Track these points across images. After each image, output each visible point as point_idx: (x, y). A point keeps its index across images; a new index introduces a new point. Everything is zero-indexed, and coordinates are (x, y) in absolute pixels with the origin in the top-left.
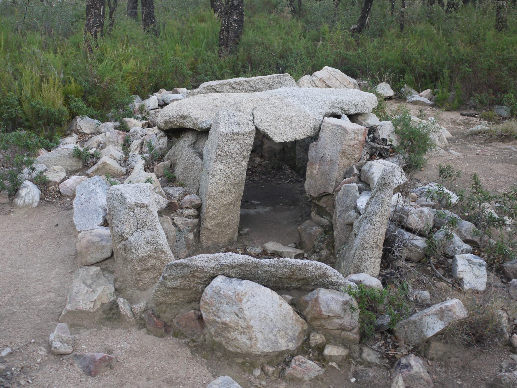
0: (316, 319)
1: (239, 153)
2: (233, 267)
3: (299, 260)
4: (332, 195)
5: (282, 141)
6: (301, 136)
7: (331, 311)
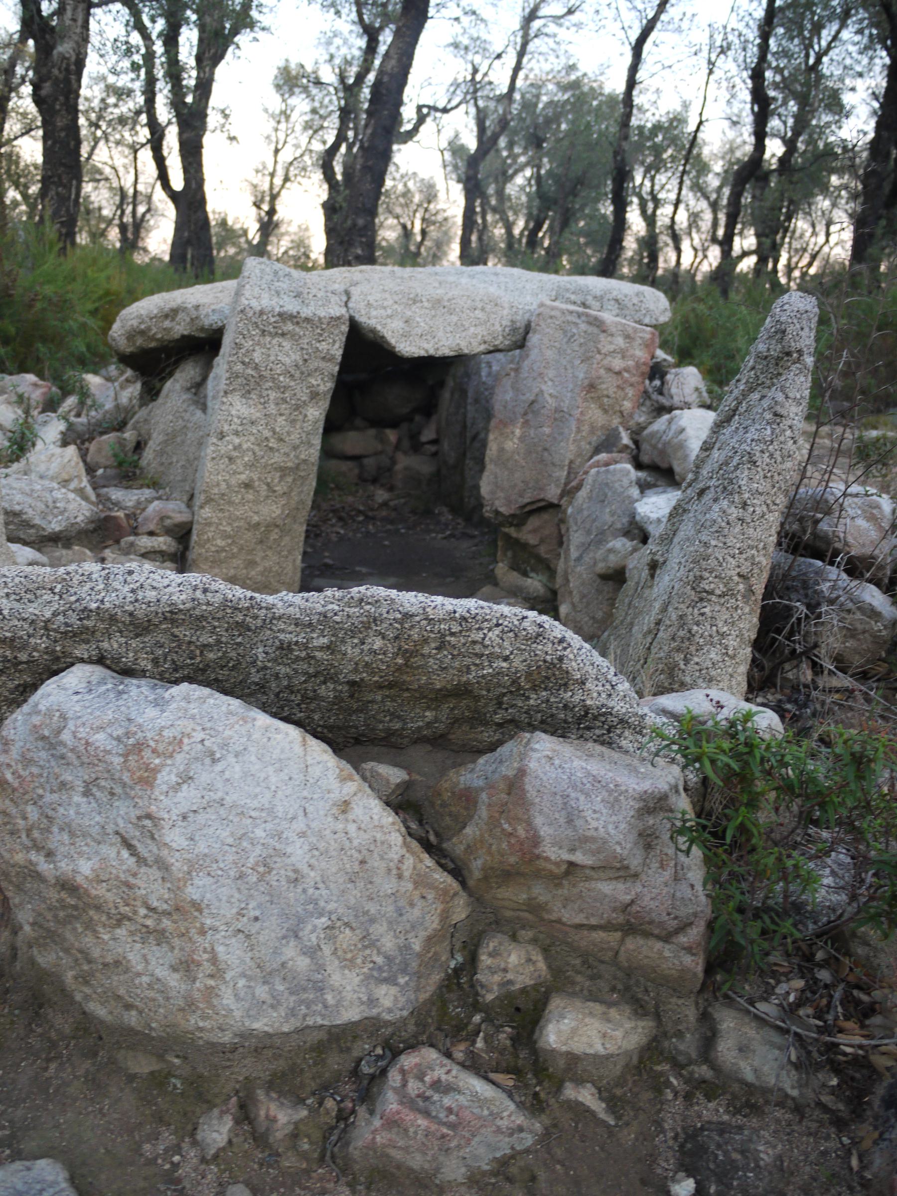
0: (508, 875)
1: (297, 375)
2: (139, 626)
3: (439, 599)
5: (423, 353)
6: (475, 344)
7: (585, 840)
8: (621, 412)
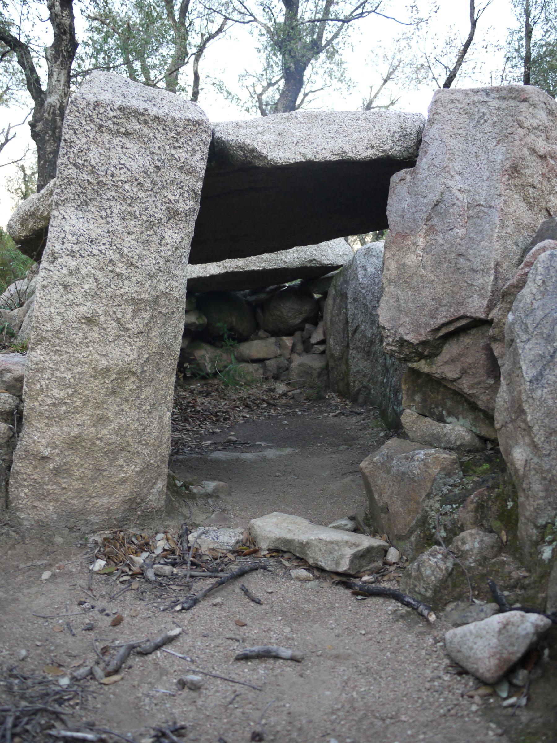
1: (148, 184)
4: (487, 323)
5: (300, 158)
6: (360, 148)
8: (547, 210)
